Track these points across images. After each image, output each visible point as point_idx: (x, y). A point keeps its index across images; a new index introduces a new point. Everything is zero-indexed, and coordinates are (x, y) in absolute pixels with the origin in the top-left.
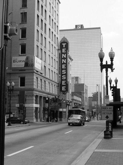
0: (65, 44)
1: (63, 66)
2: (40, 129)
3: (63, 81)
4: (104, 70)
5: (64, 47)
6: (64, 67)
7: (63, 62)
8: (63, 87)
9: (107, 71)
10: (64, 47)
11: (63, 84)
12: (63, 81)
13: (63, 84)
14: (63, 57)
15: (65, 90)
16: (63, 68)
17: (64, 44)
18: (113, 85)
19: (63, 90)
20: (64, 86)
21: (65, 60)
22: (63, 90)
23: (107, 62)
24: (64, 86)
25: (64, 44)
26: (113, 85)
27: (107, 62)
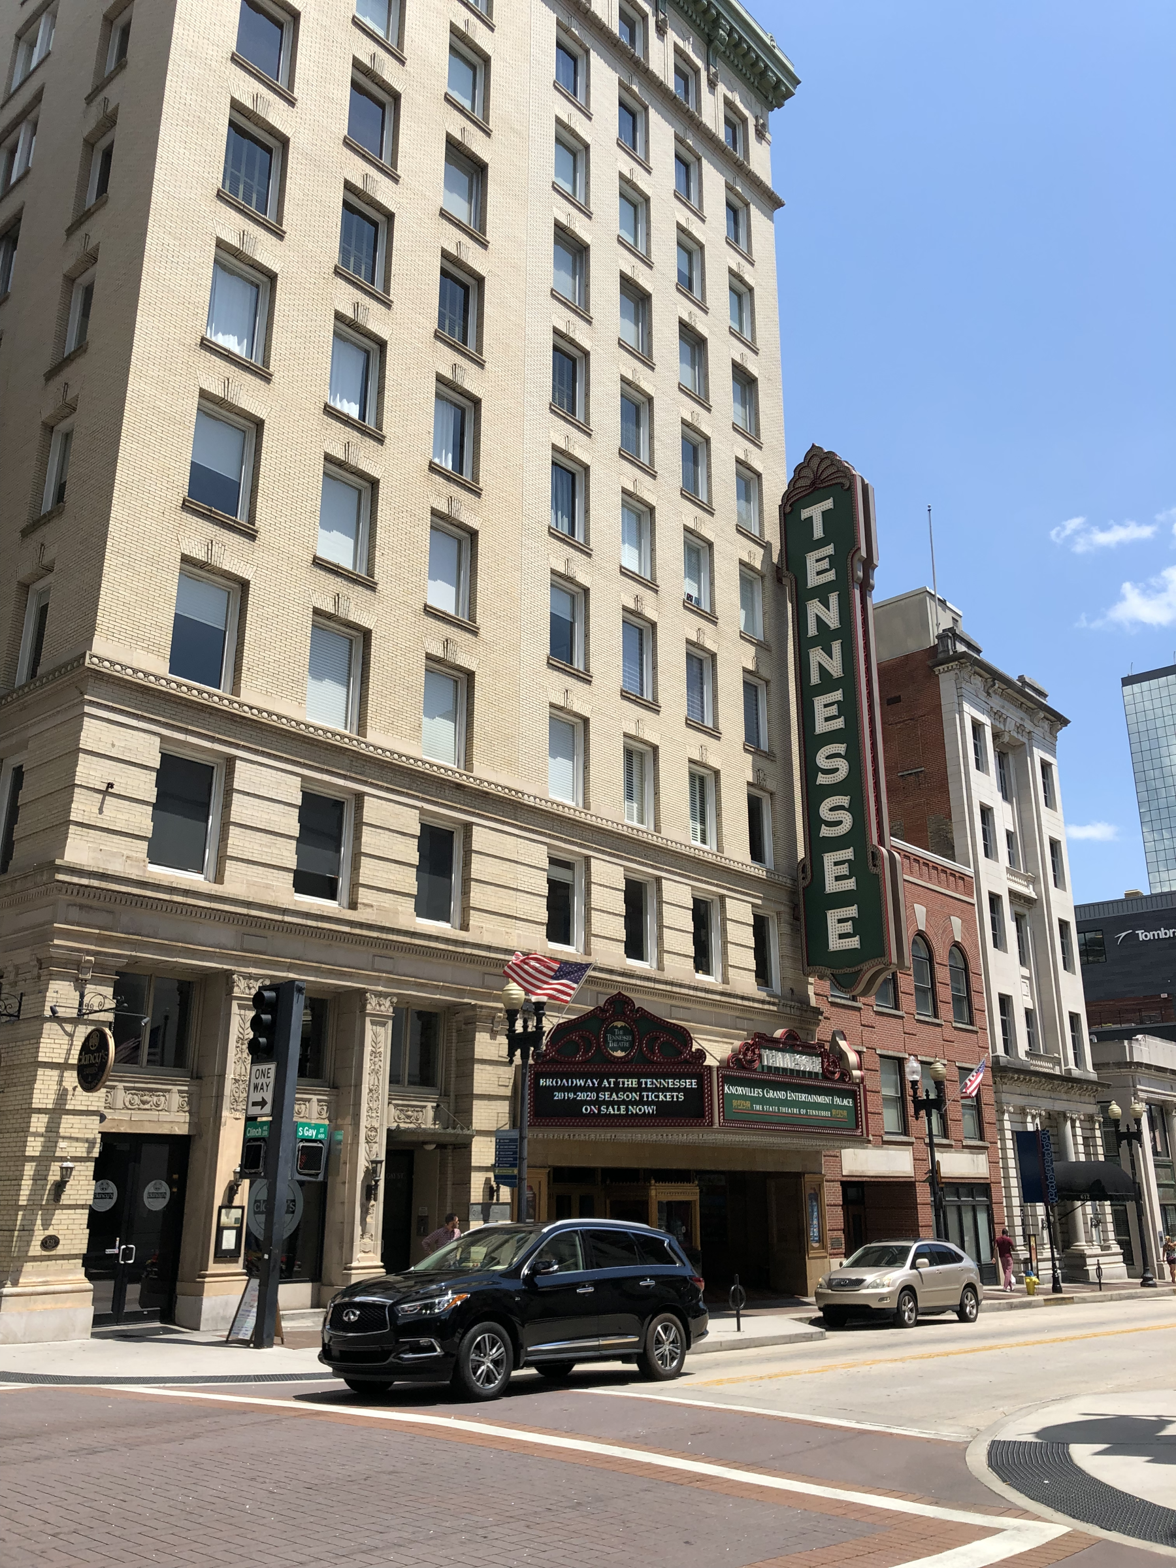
0: (828, 504)
1: (820, 712)
2: (455, 630)
3: (829, 859)
4: (1124, 1142)
5: (818, 533)
6: (842, 936)
7: (815, 679)
8: (833, 916)
9: (1130, 1144)
10: (818, 533)
11: (831, 886)
12: (829, 859)
13: (831, 886)
14: (812, 630)
15: (854, 943)
16: (821, 727)
17: (815, 513)
18: (1128, 1129)
19: (835, 944)
20: (841, 900)
21: (836, 646)
22: (835, 944)
23: (1128, 1126)
24: (841, 900)
25: (815, 513)
26: (1128, 1129)
27: (1128, 1126)
